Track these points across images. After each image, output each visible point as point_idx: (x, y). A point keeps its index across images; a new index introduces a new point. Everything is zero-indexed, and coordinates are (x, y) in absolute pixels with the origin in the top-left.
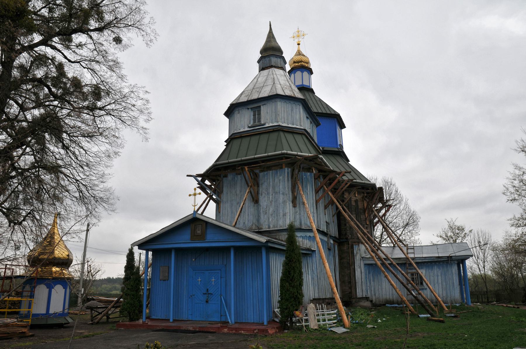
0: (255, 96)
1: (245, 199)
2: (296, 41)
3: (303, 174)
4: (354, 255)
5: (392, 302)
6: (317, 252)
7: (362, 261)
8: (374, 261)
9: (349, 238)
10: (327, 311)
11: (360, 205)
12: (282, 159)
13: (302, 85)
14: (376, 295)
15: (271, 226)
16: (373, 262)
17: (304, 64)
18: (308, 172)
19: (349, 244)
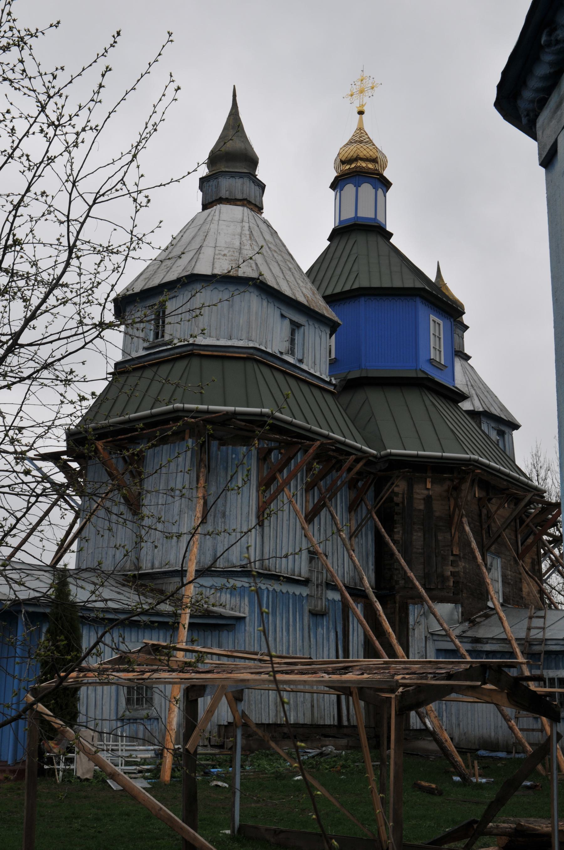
0: (155, 282)
2: (357, 104)
3: (230, 452)
5: (492, 746)
6: (247, 620)
7: (430, 644)
8: (452, 644)
9: (397, 587)
10: (126, 746)
11: (438, 509)
12: (166, 422)
14: (461, 726)
15: (157, 564)
16: (451, 646)
17: (364, 165)
18: (244, 446)
19: (395, 603)
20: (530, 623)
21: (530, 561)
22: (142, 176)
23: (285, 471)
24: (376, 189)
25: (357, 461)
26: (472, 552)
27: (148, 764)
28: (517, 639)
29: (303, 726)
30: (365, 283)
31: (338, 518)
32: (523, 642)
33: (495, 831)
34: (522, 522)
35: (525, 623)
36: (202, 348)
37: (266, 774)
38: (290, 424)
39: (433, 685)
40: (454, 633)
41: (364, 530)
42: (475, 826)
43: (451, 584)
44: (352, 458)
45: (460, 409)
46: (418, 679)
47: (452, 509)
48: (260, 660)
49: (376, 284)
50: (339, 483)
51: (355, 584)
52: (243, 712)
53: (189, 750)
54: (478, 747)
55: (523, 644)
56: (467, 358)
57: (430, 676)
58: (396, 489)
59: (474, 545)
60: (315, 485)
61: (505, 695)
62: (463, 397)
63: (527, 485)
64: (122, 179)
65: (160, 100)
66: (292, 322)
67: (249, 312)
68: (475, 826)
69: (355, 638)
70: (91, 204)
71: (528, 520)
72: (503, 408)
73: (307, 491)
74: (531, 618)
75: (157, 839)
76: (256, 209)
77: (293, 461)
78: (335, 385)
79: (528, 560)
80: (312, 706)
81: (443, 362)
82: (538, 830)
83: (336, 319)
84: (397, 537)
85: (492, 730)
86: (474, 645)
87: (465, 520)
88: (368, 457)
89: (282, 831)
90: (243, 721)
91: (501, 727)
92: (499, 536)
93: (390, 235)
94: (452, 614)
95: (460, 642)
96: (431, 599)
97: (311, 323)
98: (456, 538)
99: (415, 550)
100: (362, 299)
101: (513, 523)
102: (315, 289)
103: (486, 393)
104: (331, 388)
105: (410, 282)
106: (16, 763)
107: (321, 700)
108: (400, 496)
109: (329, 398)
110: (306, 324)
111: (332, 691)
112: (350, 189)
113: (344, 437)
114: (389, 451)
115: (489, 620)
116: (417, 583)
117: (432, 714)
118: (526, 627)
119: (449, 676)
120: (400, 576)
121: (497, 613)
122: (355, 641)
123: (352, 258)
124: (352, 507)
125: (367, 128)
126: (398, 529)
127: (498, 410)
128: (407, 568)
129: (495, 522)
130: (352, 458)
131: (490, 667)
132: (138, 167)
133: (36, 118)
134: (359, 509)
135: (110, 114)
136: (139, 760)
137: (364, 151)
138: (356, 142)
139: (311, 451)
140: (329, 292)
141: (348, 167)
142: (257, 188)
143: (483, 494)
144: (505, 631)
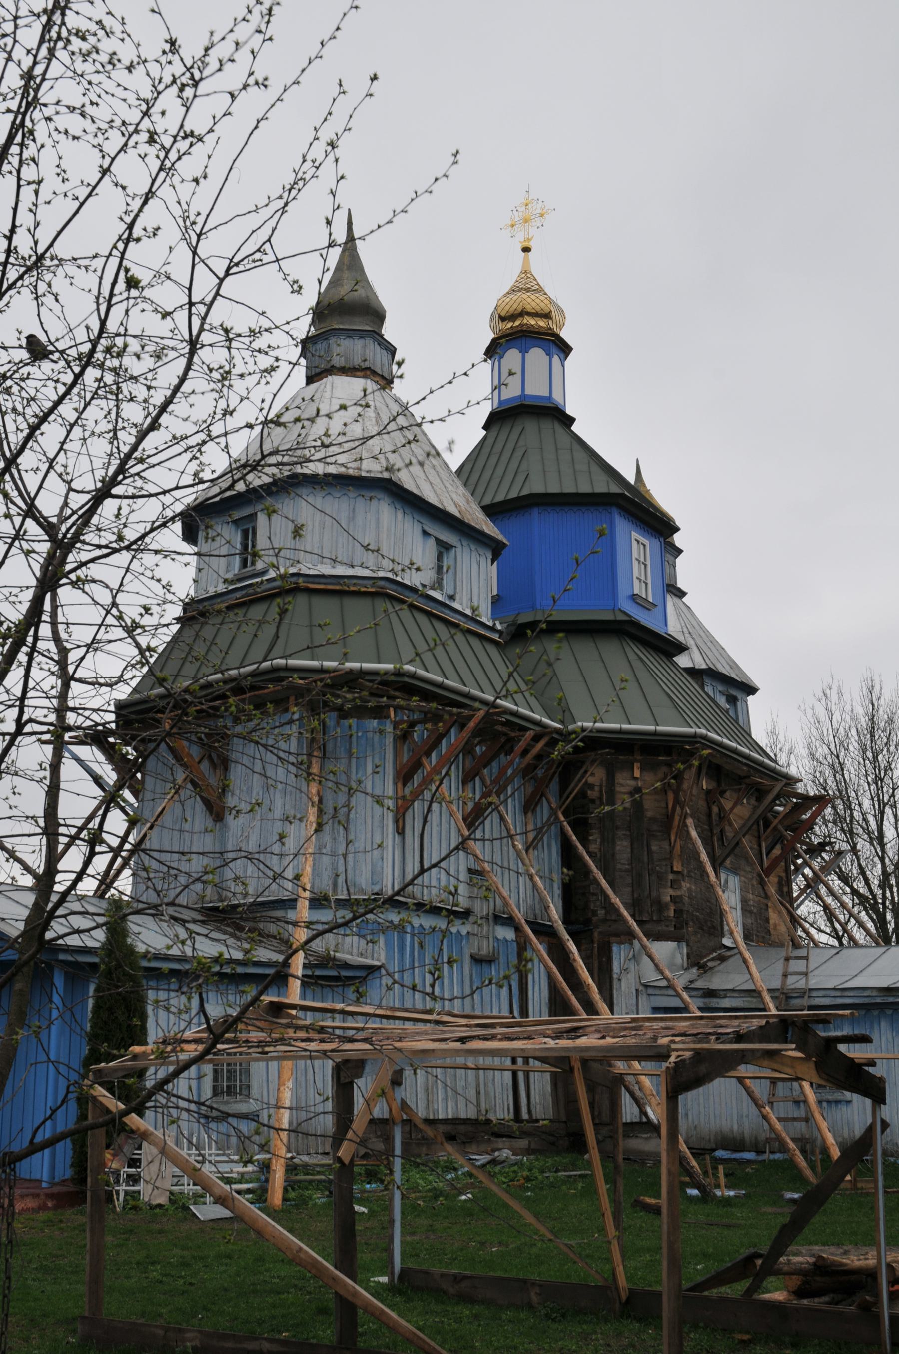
1: (162, 812)
4: (611, 978)
5: (735, 1144)
7: (643, 999)
8: (678, 999)
9: (595, 919)
10: (218, 1155)
11: (651, 807)
13: (523, 396)
16: (675, 1003)
17: (533, 322)
19: (592, 942)
20: (786, 967)
21: (776, 880)
22: (342, 178)
23: (433, 755)
24: (549, 354)
25: (537, 738)
26: (701, 867)
27: (247, 1182)
28: (769, 991)
29: (466, 1121)
30: (537, 487)
31: (509, 819)
32: (777, 994)
33: (786, 1268)
34: (767, 824)
35: (779, 966)
36: (311, 579)
37: (420, 1191)
38: (440, 686)
39: (719, 1051)
40: (680, 984)
41: (545, 839)
42: (759, 1262)
43: (672, 914)
44: (529, 735)
45: (675, 665)
46: (694, 1042)
47: (670, 807)
48: (437, 1022)
49: (554, 489)
50: (510, 772)
51: (535, 915)
52: (403, 1102)
53: (343, 1158)
54: (714, 1146)
55: (777, 997)
56: (681, 594)
57: (713, 1037)
58: (591, 780)
59: (704, 857)
60: (477, 775)
61: (812, 1065)
62: (681, 648)
63: (773, 771)
64: (269, 240)
65: (325, 120)
66: (439, 542)
67: (378, 527)
68: (759, 1262)
69: (537, 994)
70: (221, 275)
71: (776, 821)
72: (734, 665)
73: (465, 783)
74: (787, 959)
75: (279, 1293)
76: (382, 382)
77: (444, 742)
78: (500, 632)
79: (773, 879)
80: (478, 1093)
81: (650, 599)
82: (846, 1265)
83: (500, 537)
84: (593, 847)
85: (735, 1122)
86: (707, 1000)
87: (690, 822)
88: (551, 733)
89: (465, 1277)
90: (405, 1117)
91: (747, 1116)
92: (737, 844)
93: (572, 420)
94: (673, 956)
95: (690, 997)
96: (646, 936)
97: (465, 543)
98: (678, 848)
99: (619, 866)
100: (535, 511)
101: (755, 827)
102: (468, 494)
103: (709, 644)
104: (496, 636)
105: (602, 485)
106: (52, 1184)
107: (490, 1085)
108: (597, 789)
109: (493, 650)
110: (458, 545)
111: (547, 1067)
112: (512, 357)
113: (516, 705)
114: (580, 724)
115: (725, 964)
116: (625, 913)
117: (653, 1099)
118: (780, 973)
119: (739, 1037)
120: (598, 903)
121: (741, 954)
122: (537, 999)
123: (519, 453)
124: (529, 807)
125: (536, 271)
126: (594, 836)
127: (727, 667)
128: (610, 892)
129: (731, 825)
130: (529, 735)
131: (793, 1023)
132: (337, 161)
133: (138, 125)
134: (538, 809)
135: (258, 122)
136: (234, 1175)
137: (532, 302)
138: (520, 290)
139: (472, 724)
140: (487, 501)
141: (510, 325)
142: (384, 352)
143: (712, 785)
144: (752, 977)
